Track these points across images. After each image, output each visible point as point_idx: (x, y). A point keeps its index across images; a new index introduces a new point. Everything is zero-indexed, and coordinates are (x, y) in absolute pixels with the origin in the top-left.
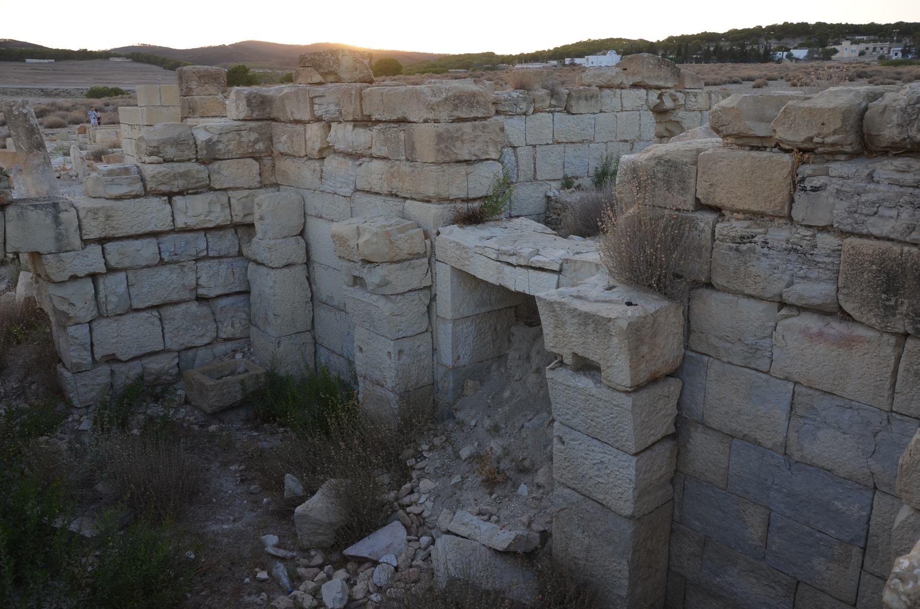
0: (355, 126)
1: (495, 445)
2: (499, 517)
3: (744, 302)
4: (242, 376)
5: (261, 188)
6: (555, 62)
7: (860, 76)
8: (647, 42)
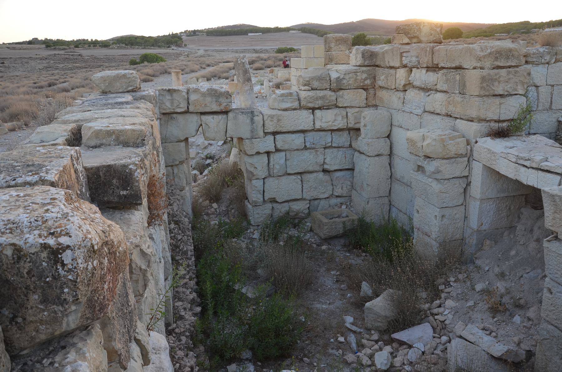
0: (427, 71)
1: (501, 286)
2: (497, 334)
4: (344, 219)
5: (366, 107)
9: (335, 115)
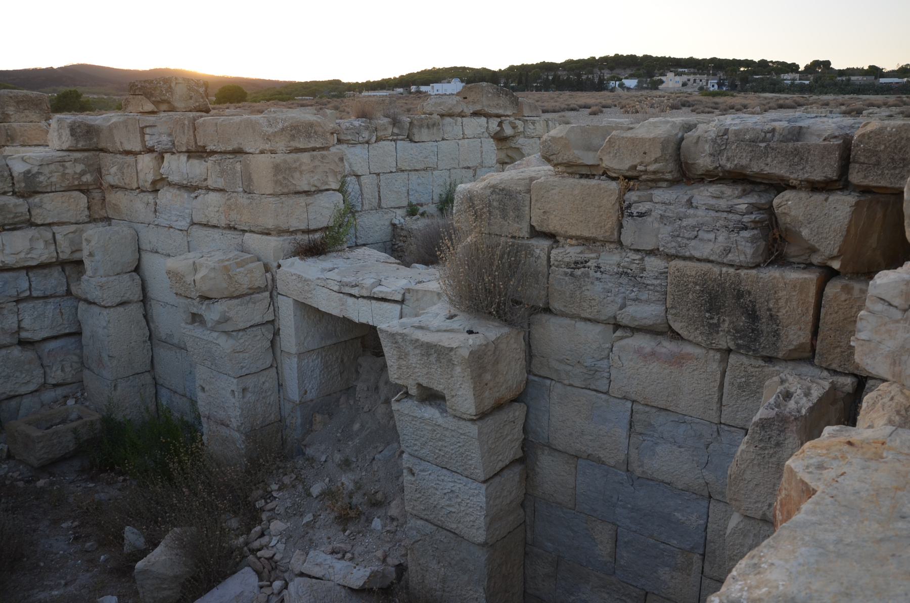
0: (189, 157)
1: (347, 480)
2: (353, 554)
3: (581, 325)
4: (75, 424)
6: (401, 90)
7: (684, 105)
8: (490, 71)
9: (31, 240)
